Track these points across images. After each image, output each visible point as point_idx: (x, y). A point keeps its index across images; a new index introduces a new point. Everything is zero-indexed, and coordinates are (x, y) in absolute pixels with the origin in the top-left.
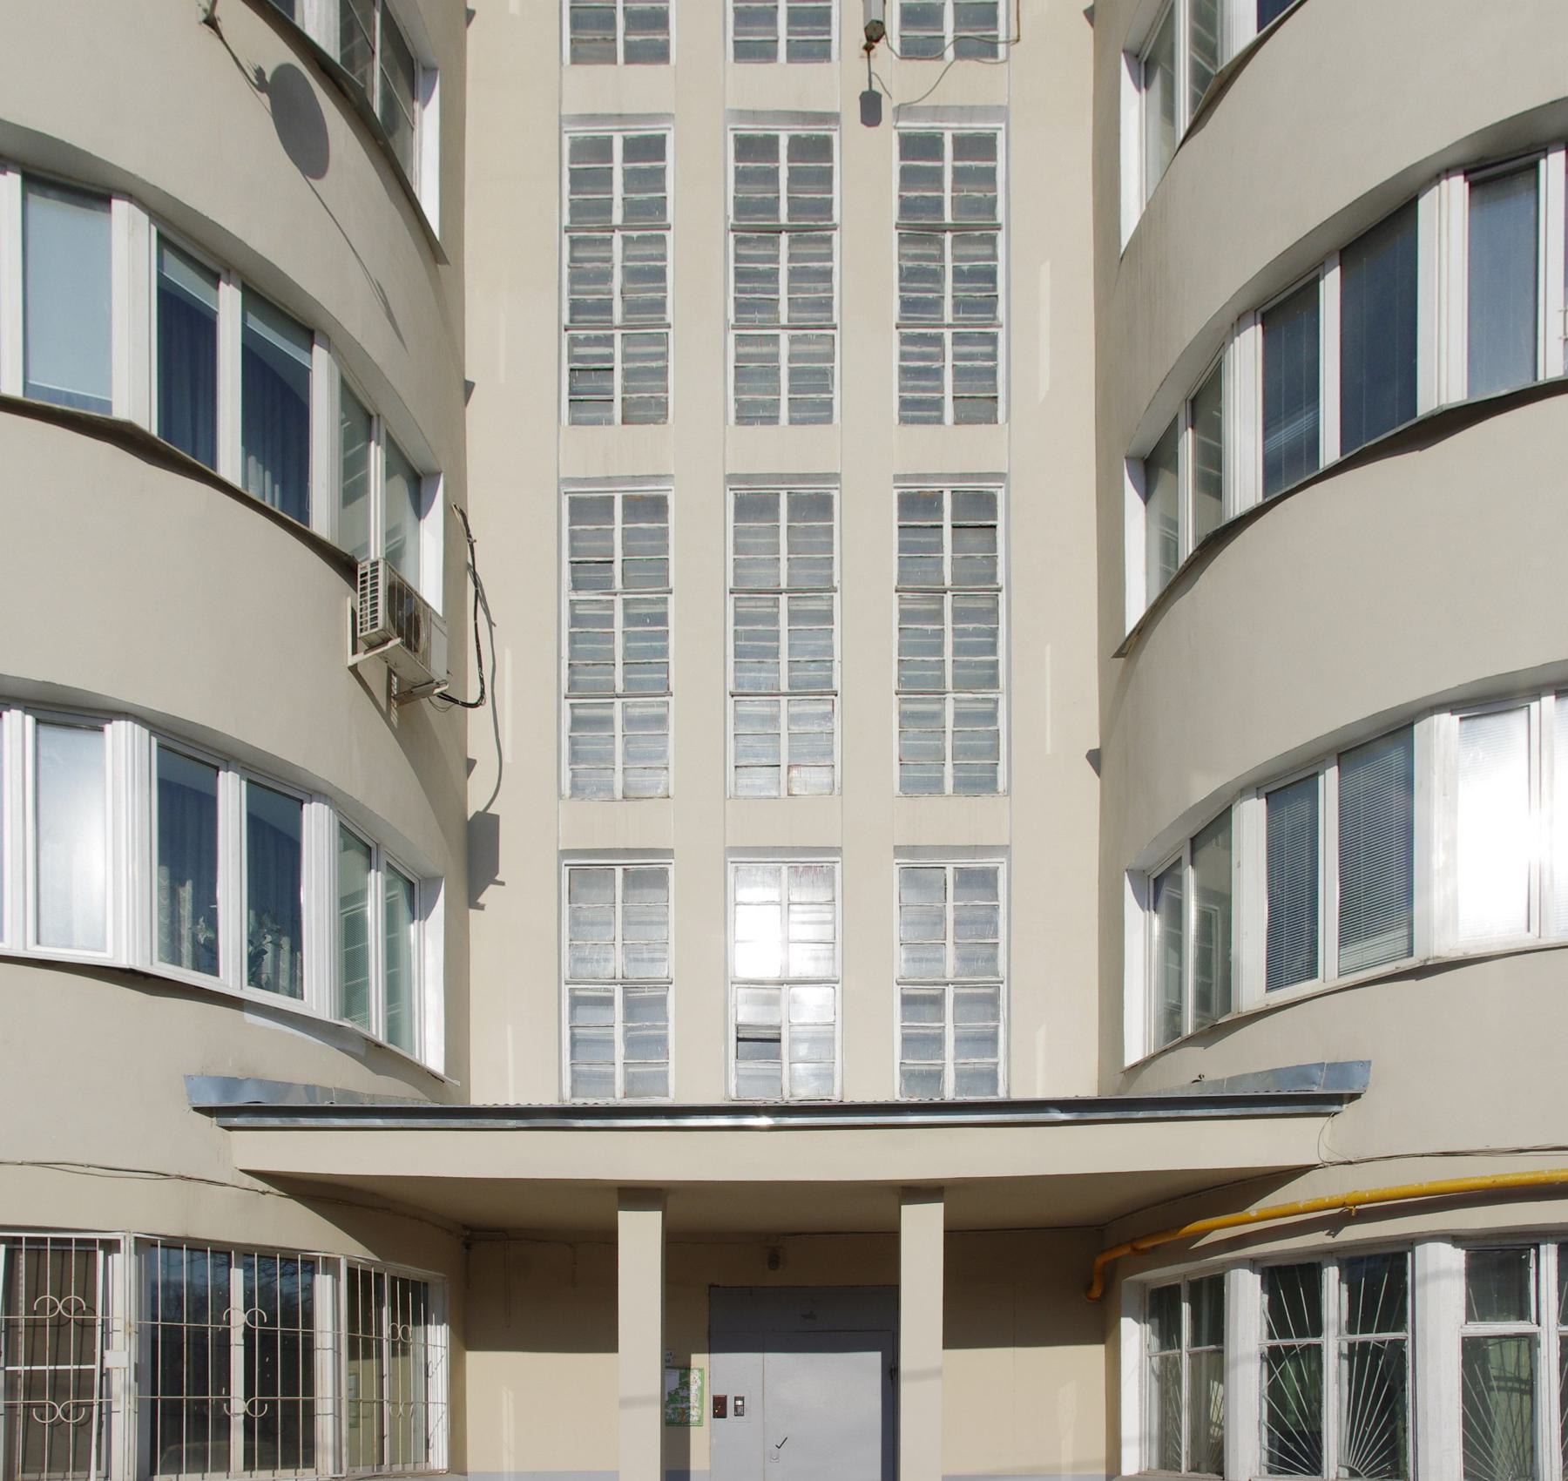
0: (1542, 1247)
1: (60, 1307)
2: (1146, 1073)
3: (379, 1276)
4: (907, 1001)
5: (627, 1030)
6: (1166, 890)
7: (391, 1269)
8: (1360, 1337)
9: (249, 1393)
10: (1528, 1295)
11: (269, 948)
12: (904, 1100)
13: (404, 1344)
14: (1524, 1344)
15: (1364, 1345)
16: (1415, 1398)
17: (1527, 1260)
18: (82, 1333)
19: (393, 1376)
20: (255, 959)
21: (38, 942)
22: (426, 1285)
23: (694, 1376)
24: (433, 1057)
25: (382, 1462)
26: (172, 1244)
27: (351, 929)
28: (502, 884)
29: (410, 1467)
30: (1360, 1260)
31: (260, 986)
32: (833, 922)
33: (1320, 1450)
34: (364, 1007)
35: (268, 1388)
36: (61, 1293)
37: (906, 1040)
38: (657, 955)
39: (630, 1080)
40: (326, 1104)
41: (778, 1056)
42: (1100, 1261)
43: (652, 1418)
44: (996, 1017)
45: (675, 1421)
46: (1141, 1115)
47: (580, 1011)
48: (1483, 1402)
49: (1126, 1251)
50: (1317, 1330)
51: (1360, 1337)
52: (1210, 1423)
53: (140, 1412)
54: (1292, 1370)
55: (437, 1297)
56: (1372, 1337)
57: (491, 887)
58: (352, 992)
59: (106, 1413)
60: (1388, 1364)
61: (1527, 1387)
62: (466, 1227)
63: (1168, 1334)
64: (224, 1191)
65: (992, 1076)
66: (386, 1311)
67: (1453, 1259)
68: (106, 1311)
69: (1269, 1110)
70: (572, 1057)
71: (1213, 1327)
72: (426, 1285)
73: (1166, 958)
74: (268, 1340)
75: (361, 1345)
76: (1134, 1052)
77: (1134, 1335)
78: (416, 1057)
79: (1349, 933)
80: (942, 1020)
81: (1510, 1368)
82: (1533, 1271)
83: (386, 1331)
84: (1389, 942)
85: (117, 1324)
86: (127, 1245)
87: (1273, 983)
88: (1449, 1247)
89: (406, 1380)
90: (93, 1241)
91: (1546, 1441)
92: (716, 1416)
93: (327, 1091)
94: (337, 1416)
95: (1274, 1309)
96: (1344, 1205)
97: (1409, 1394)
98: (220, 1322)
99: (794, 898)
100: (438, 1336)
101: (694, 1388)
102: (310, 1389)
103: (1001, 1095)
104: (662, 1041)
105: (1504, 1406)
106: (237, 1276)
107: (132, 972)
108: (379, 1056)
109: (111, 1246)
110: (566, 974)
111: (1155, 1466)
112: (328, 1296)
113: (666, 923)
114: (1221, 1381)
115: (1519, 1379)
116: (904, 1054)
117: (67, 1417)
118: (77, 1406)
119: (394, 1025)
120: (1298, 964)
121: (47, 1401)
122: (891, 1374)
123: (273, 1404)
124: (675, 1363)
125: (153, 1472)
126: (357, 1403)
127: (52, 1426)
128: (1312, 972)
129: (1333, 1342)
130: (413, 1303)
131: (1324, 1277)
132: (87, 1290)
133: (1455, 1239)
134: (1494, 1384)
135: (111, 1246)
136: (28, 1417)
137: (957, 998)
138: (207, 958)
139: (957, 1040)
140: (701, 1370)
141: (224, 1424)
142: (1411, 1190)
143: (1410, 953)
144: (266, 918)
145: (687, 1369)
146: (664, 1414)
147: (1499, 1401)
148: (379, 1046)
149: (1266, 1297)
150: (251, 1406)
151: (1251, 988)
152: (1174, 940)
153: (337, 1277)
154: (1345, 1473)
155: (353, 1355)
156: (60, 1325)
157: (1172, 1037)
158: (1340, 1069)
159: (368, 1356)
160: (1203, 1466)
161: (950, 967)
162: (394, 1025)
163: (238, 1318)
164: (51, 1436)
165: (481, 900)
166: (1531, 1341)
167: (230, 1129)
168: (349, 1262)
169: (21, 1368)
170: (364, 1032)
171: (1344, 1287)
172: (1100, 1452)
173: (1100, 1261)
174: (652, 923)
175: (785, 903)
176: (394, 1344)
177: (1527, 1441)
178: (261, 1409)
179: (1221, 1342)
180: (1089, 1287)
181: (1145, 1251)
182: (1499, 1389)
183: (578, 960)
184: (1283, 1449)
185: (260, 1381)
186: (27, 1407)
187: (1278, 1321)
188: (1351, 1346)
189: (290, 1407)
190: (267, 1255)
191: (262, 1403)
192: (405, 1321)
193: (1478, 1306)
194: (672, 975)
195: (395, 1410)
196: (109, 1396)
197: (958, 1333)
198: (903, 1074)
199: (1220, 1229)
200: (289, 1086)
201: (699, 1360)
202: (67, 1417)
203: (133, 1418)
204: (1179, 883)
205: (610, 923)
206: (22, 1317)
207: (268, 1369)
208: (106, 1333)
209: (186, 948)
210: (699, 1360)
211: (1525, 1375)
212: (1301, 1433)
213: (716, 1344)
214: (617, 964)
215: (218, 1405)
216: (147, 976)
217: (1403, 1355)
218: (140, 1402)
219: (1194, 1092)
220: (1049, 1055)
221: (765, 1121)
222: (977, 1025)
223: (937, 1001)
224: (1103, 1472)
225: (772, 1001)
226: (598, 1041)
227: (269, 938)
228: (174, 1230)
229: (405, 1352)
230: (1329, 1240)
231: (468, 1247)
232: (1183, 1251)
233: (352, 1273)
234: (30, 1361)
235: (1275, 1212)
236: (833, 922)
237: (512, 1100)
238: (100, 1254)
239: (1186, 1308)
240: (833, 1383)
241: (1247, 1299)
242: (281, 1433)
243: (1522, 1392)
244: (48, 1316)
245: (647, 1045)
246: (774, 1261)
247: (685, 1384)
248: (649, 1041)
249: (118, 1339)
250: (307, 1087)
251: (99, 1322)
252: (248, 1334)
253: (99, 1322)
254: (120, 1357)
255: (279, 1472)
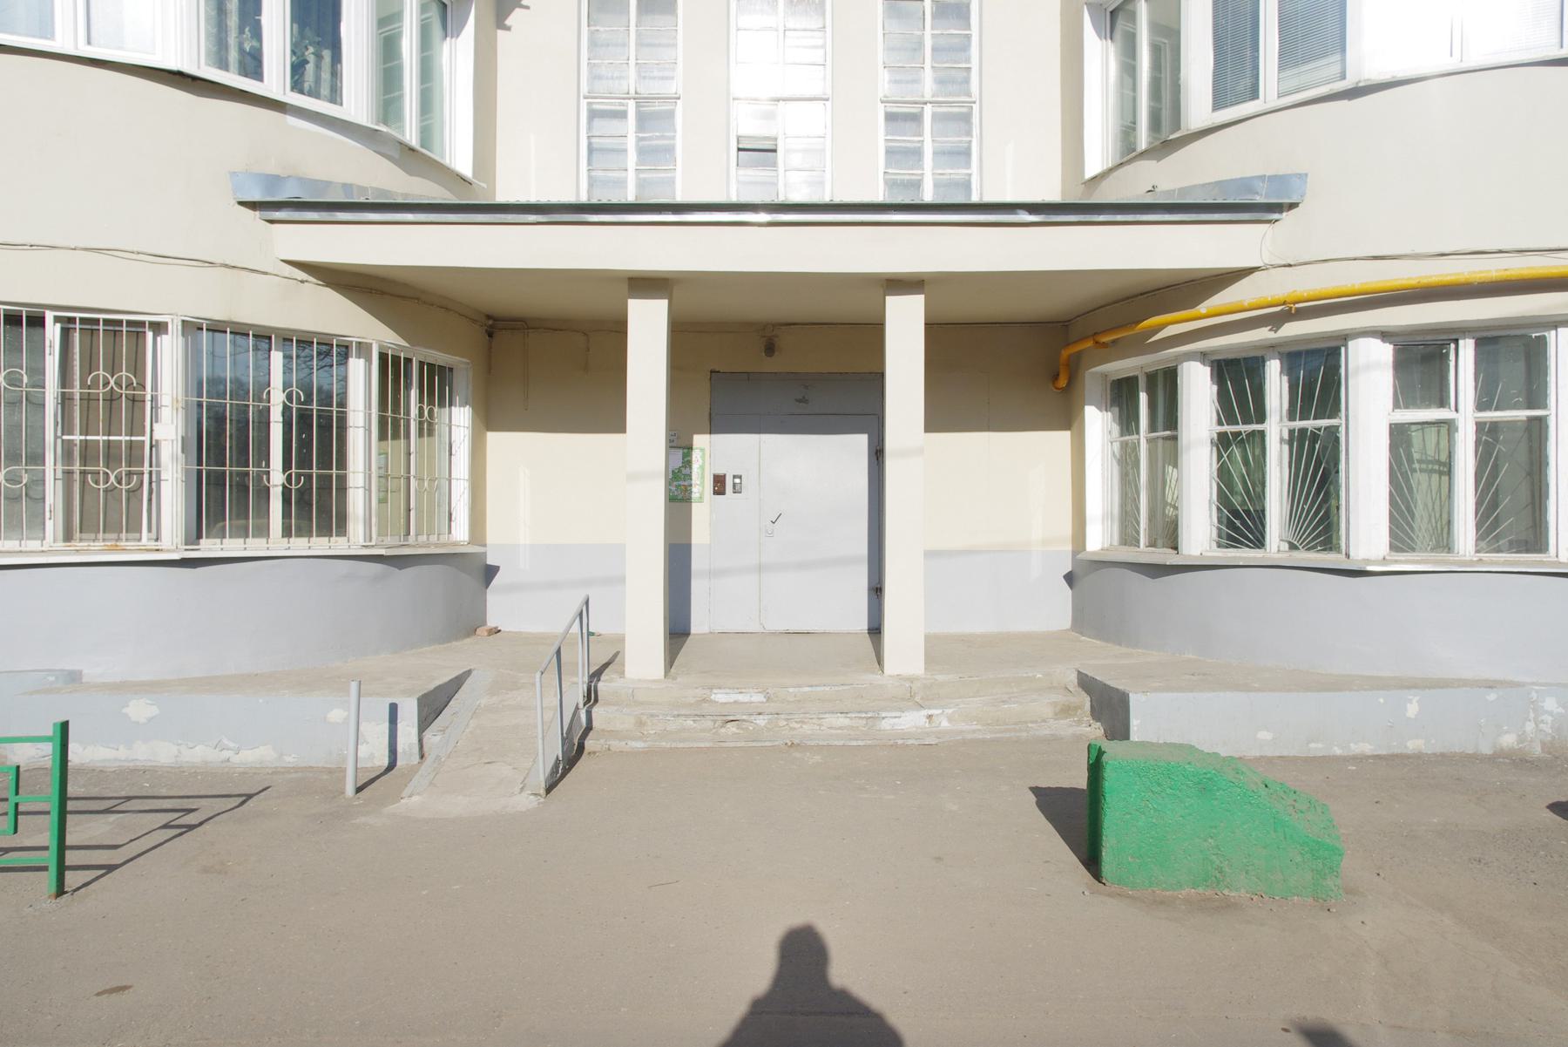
0: (1461, 342)
1: (112, 382)
2: (1105, 184)
3: (408, 361)
4: (891, 118)
5: (639, 139)
6: (1121, 23)
7: (420, 354)
8: (1299, 424)
9: (287, 465)
10: (1447, 385)
11: (311, 58)
12: (889, 201)
13: (430, 424)
14: (1444, 430)
15: (1303, 431)
16: (1347, 478)
17: (1447, 354)
18: (131, 407)
19: (420, 452)
20: (298, 69)
21: (89, 43)
22: (451, 370)
23: (696, 455)
24: (463, 163)
25: (408, 533)
26: (216, 328)
27: (388, 48)
28: (527, 8)
29: (434, 538)
30: (1298, 354)
31: (301, 92)
32: (824, 46)
33: (1264, 526)
34: (399, 117)
35: (304, 462)
36: (113, 368)
37: (889, 152)
38: (666, 74)
39: (641, 184)
40: (362, 200)
41: (774, 164)
42: (1065, 353)
43: (655, 493)
44: (969, 133)
45: (678, 496)
46: (1101, 218)
47: (597, 123)
48: (1407, 481)
49: (1090, 344)
50: (1261, 418)
51: (1299, 424)
52: (1165, 504)
53: (187, 482)
54: (1238, 449)
55: (463, 381)
56: (1310, 424)
57: (518, 11)
58: (388, 102)
59: (156, 481)
60: (1324, 448)
61: (1446, 468)
62: (489, 317)
63: (1128, 422)
64: (266, 279)
65: (967, 185)
66: (414, 393)
67: (1383, 353)
68: (155, 387)
69: (1216, 217)
70: (589, 163)
71: (1168, 415)
72: (451, 370)
73: (1121, 83)
74: (305, 417)
75: (390, 426)
76: (1093, 167)
77: (1098, 422)
78: (447, 162)
79: (1288, 58)
80: (921, 134)
81: (1431, 451)
82: (1452, 364)
83: (414, 411)
84: (1328, 66)
85: (166, 399)
86: (175, 327)
87: (1219, 103)
88: (1378, 342)
89: (431, 457)
90: (142, 324)
91: (1462, 515)
92: (716, 493)
93: (363, 189)
94: (368, 490)
95: (1222, 396)
96: (1284, 303)
97: (1342, 474)
98: (260, 400)
99: (790, 25)
100: (460, 418)
101: (695, 467)
102: (342, 464)
103: (975, 199)
104: (670, 150)
105: (1424, 486)
106: (277, 358)
107: (180, 74)
108: (411, 158)
109: (159, 328)
110: (584, 89)
111: (1116, 542)
112: (360, 380)
113: (675, 45)
114: (1175, 465)
115: (1439, 463)
116: (888, 164)
117: (120, 483)
118: (129, 474)
119: (426, 133)
120: (1241, 88)
121: (102, 468)
122: (877, 454)
123: (309, 477)
124: (679, 443)
125: (199, 536)
126: (386, 477)
127: (106, 491)
128: (1254, 94)
129: (1276, 428)
130: (438, 384)
131: (1267, 369)
132: (137, 366)
133: (1384, 335)
134: (1416, 466)
135: (159, 328)
136: (84, 482)
137: (934, 116)
138: (253, 64)
139: (935, 153)
140: (702, 450)
141: (265, 493)
142: (1345, 290)
143: (1343, 77)
144: (308, 32)
145: (689, 448)
146: (668, 491)
147: (1422, 482)
148: (412, 150)
149: (1215, 388)
150: (289, 479)
151: (1198, 108)
152: (1129, 68)
153: (369, 360)
154: (1285, 546)
155: (383, 436)
156: (112, 399)
157: (1129, 153)
158: (1279, 180)
159: (396, 436)
160: (1160, 542)
161: (928, 87)
162: (426, 133)
163: (277, 398)
164: (106, 499)
165: (508, 22)
166: (1449, 426)
167: (272, 222)
168: (380, 347)
169: (77, 438)
170: (399, 137)
171: (1285, 378)
172: (1066, 528)
173: (1065, 353)
174: (660, 45)
175: (781, 29)
176: (421, 423)
177: (1445, 516)
178: (298, 481)
179: (1176, 428)
180: (1056, 377)
181: (1105, 345)
182: (1421, 470)
183: (595, 77)
184: (1231, 525)
185: (297, 456)
186: (83, 473)
187: (1226, 411)
188: (1291, 432)
189: (325, 482)
190: (304, 342)
191: (299, 476)
192: (431, 402)
193: (1405, 395)
194: (680, 92)
195: (421, 485)
196: (158, 465)
197: (939, 417)
198: (886, 182)
199: (1174, 324)
200: (328, 184)
201: (701, 441)
202: (120, 483)
203: (181, 487)
204: (1132, 17)
205: (625, 45)
206: (77, 391)
207: (305, 445)
208: (155, 408)
209: (233, 55)
210: (701, 441)
211: (1443, 458)
212: (1248, 512)
213: (716, 425)
214: (631, 82)
215: (259, 477)
216: (195, 78)
217: (1337, 440)
218: (187, 472)
219: (1149, 200)
220: (1020, 166)
221: (763, 217)
222: (953, 140)
223: (916, 118)
224: (1069, 548)
225: (769, 116)
226: (613, 150)
227: (311, 49)
228: (218, 314)
229: (431, 433)
230: (1272, 335)
231: (490, 335)
232: (1141, 345)
233: (383, 357)
234: (85, 431)
235: (1223, 309)
236: (824, 46)
237: (533, 199)
238: (150, 335)
239: (1143, 398)
240: (817, 464)
241: (1198, 391)
242: (317, 506)
243: (1441, 473)
244: (101, 390)
245: (655, 154)
246: (770, 349)
247: (688, 463)
248: (656, 150)
249: (166, 413)
250: (344, 185)
251: (148, 397)
252: (286, 410)
253: (148, 397)
254: (169, 430)
255: (334, 539)
